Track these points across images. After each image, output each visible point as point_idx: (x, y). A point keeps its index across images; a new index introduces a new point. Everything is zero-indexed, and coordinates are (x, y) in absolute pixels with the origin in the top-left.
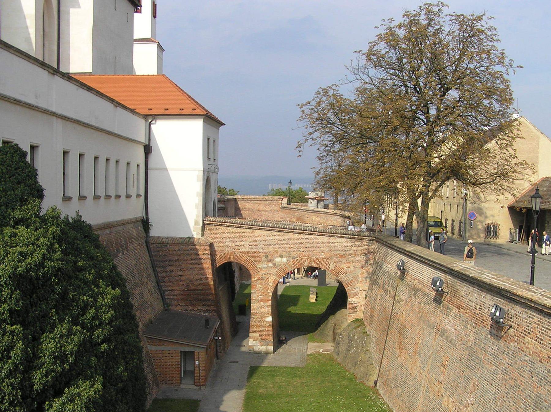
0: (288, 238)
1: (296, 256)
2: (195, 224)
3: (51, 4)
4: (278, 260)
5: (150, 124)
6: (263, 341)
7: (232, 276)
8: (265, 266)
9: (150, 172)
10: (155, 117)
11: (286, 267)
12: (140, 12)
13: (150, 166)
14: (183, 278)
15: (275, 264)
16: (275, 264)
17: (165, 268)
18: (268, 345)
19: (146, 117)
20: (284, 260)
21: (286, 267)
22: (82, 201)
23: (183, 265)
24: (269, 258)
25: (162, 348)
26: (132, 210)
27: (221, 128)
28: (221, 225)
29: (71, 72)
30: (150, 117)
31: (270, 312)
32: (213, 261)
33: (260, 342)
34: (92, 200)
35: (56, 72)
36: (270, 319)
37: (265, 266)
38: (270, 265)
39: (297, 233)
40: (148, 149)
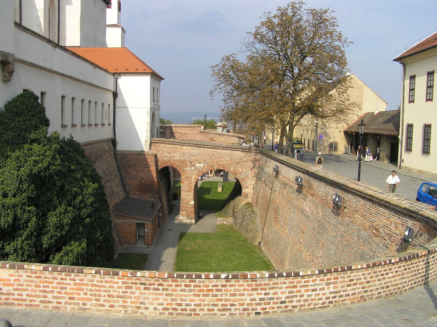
4: (198, 165)
6: (188, 217)
8: (190, 169)
9: (117, 110)
10: (120, 74)
11: (203, 170)
14: (138, 177)
15: (196, 168)
16: (196, 168)
17: (126, 170)
18: (191, 219)
19: (114, 74)
20: (202, 165)
21: (203, 170)
23: (138, 168)
24: (192, 164)
28: (162, 143)
30: (117, 74)
31: (193, 198)
32: (157, 166)
33: (187, 217)
36: (193, 203)
38: (193, 168)
39: (210, 148)
40: (115, 95)
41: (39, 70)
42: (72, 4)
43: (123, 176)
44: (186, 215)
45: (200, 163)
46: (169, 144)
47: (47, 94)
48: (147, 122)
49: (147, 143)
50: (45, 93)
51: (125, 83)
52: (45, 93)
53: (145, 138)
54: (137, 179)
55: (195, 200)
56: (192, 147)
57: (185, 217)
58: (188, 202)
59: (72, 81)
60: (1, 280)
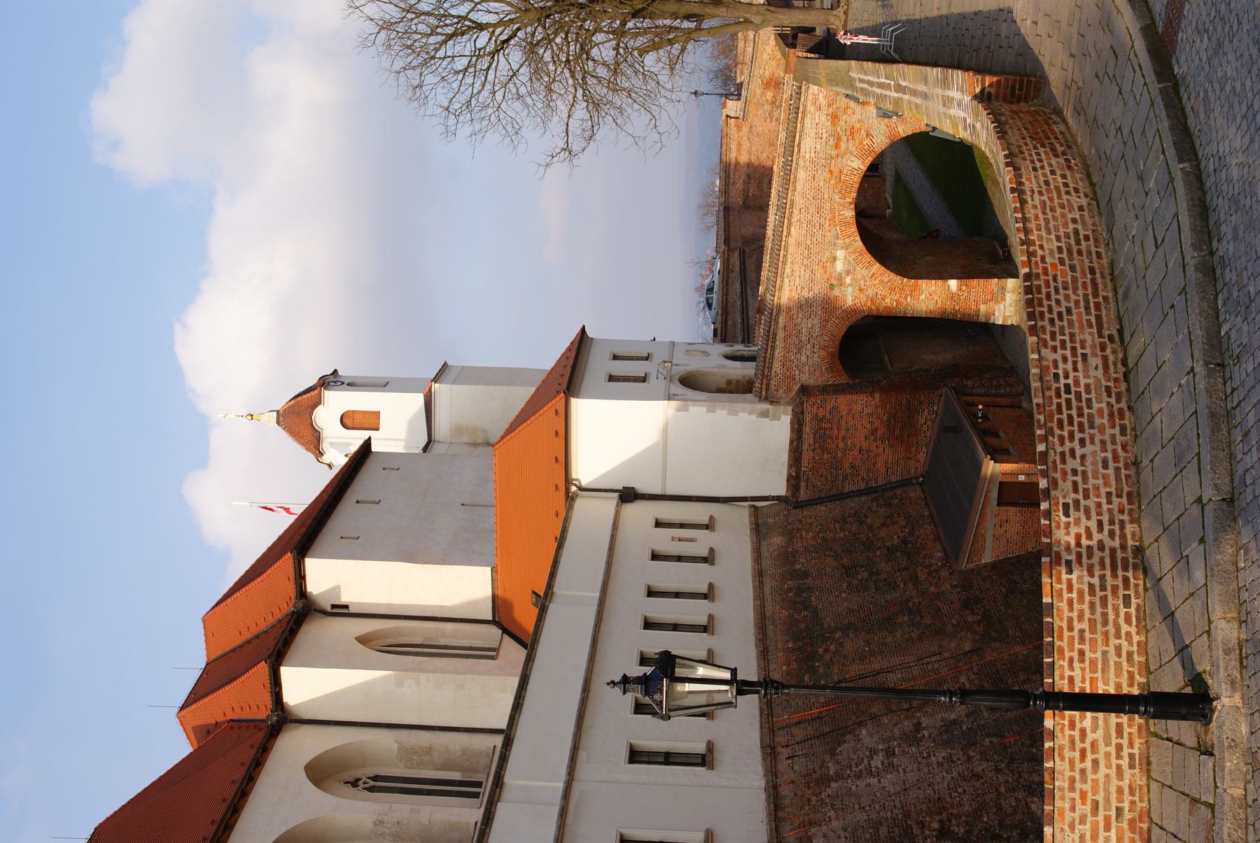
0: (799, 244)
1: (833, 233)
2: (767, 416)
3: (377, 632)
4: (839, 266)
5: (581, 489)
6: (999, 297)
7: (866, 343)
8: (850, 289)
9: (670, 492)
10: (568, 481)
11: (854, 252)
12: (377, 414)
13: (658, 491)
14: (865, 445)
15: (848, 272)
16: (848, 272)
17: (845, 477)
18: (1003, 288)
19: (570, 499)
20: (840, 254)
21: (854, 252)
22: (717, 560)
23: (841, 445)
24: (834, 282)
25: (989, 539)
26: (734, 541)
27: (590, 333)
28: (770, 368)
29: (489, 593)
30: (569, 492)
31: (940, 282)
32: (837, 389)
33: (997, 302)
34: (715, 721)
35: (508, 736)
36: (953, 284)
37: (850, 289)
38: (848, 280)
39: (789, 229)
40: (628, 495)
41: (591, 694)
42: (338, 587)
43: (862, 486)
44: (992, 304)
45: (835, 259)
46: (773, 348)
47: (634, 742)
48: (708, 411)
49: (768, 411)
50: (646, 618)
51: (590, 463)
52: (646, 618)
53: (754, 417)
54: (873, 447)
55: (943, 276)
56: (786, 281)
57: (1002, 303)
58: (952, 296)
59: (601, 638)
60: (1095, 837)
